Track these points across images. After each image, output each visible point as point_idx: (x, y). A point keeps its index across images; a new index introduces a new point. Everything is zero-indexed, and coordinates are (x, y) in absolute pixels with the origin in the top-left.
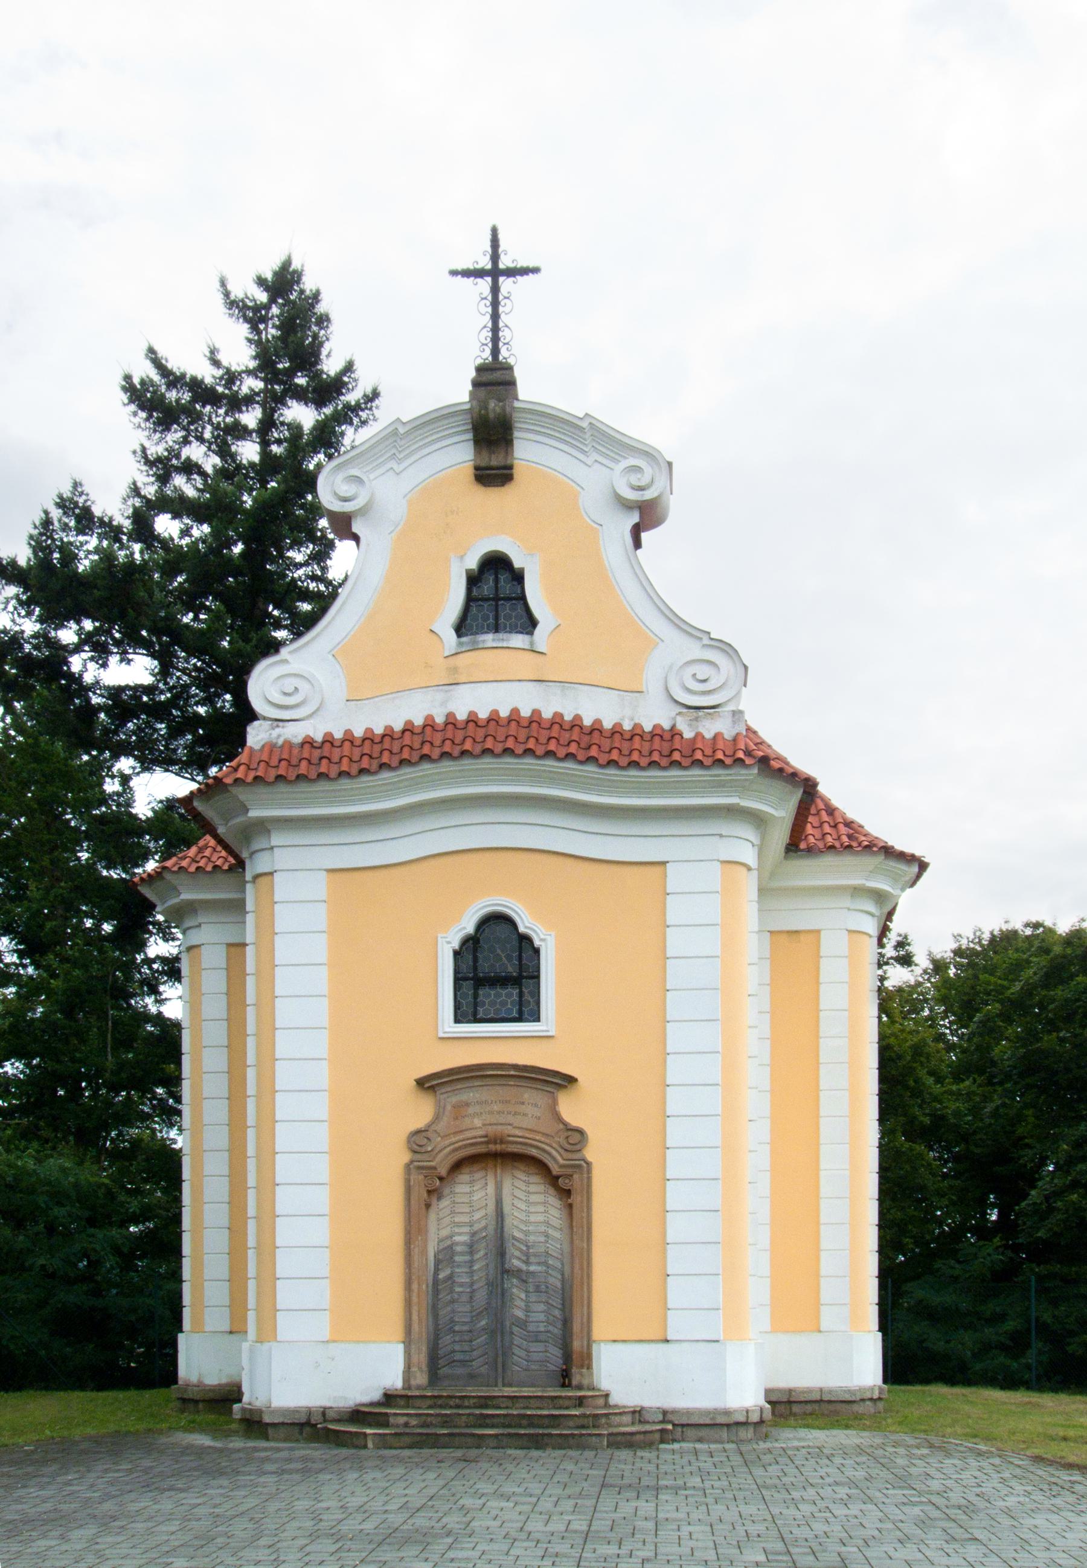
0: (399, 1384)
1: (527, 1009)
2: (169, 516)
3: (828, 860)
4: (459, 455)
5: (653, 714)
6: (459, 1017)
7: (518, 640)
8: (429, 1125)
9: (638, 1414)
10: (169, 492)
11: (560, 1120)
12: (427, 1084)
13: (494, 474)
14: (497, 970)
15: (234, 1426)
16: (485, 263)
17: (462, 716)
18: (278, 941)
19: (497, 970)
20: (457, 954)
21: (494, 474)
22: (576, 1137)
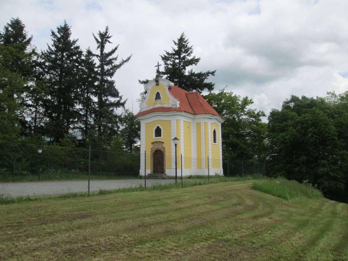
0: (150, 173)
1: (160, 136)
2: (195, 73)
3: (199, 115)
4: (155, 83)
5: (170, 106)
6: (155, 137)
7: (159, 100)
8: (153, 147)
9: (168, 176)
10: (103, 99)
11: (162, 146)
12: (153, 143)
13: (157, 85)
14: (158, 132)
15: (143, 177)
16: (157, 65)
17: (155, 108)
18: (171, 124)
19: (158, 132)
20: (155, 130)
21: (157, 85)
22: (164, 148)
